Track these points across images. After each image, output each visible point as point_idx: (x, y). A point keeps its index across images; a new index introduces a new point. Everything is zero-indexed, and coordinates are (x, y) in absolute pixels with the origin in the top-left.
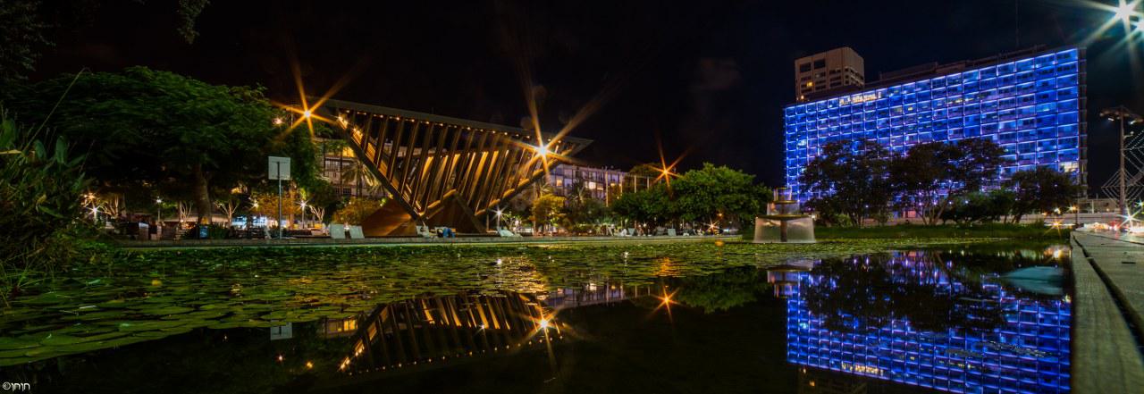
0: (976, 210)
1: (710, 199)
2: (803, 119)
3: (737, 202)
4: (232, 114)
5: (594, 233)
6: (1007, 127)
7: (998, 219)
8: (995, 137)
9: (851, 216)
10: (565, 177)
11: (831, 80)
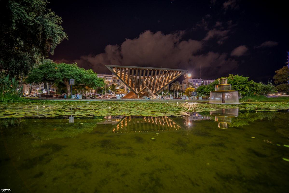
3: (239, 88)
10: (198, 83)
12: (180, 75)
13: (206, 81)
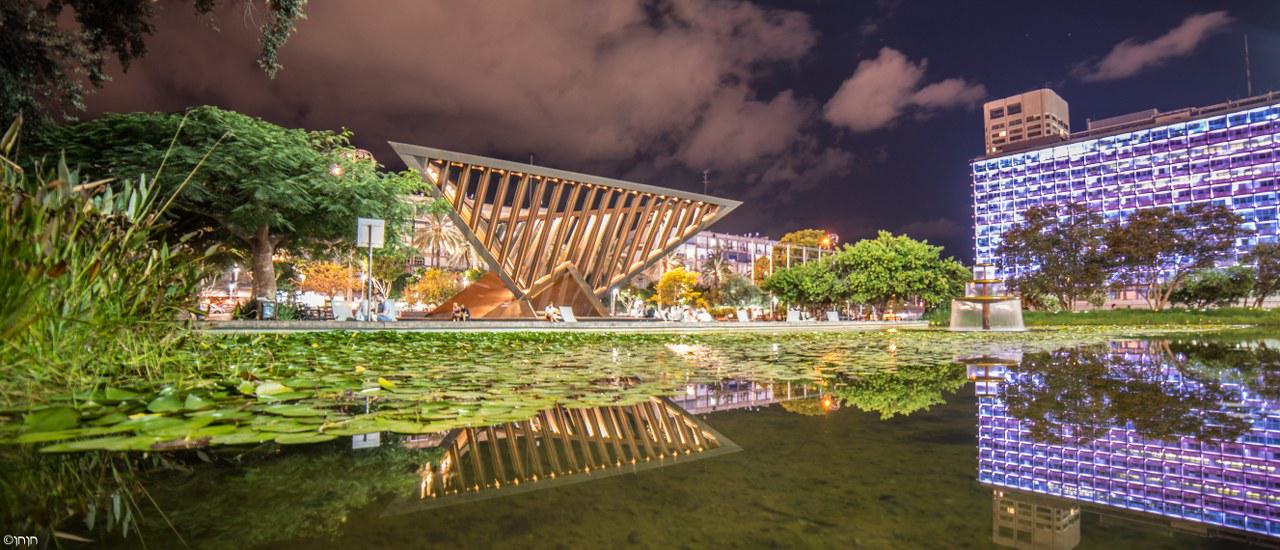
0: (1209, 292)
1: (888, 276)
2: (995, 177)
3: (921, 280)
4: (314, 165)
5: (461, 319)
6: (1243, 189)
7: (1237, 302)
8: (1228, 201)
9: (1061, 298)
10: (698, 246)
11: (1029, 129)
12: (710, 220)
13: (726, 241)
